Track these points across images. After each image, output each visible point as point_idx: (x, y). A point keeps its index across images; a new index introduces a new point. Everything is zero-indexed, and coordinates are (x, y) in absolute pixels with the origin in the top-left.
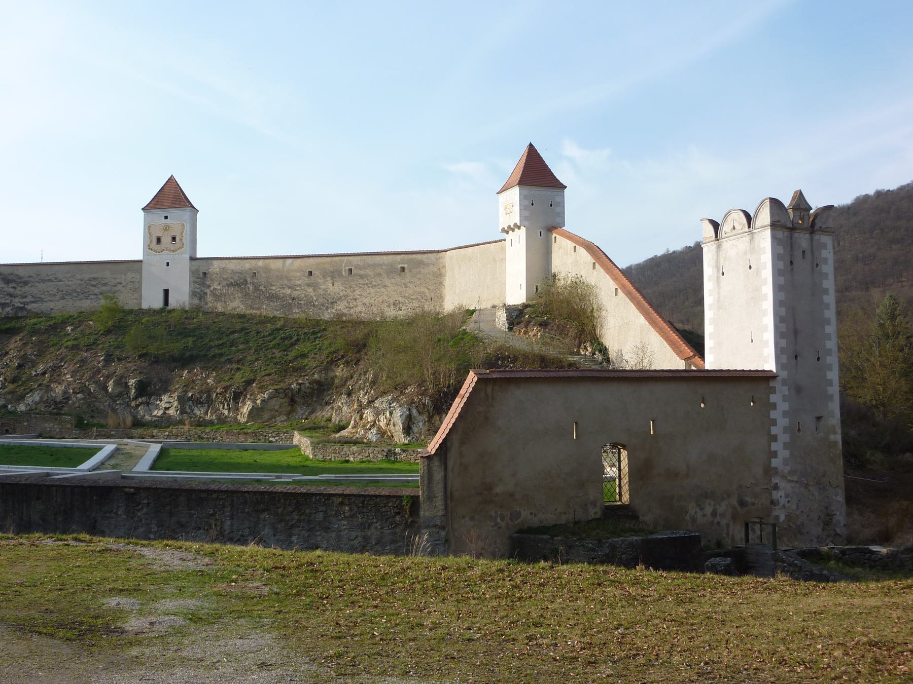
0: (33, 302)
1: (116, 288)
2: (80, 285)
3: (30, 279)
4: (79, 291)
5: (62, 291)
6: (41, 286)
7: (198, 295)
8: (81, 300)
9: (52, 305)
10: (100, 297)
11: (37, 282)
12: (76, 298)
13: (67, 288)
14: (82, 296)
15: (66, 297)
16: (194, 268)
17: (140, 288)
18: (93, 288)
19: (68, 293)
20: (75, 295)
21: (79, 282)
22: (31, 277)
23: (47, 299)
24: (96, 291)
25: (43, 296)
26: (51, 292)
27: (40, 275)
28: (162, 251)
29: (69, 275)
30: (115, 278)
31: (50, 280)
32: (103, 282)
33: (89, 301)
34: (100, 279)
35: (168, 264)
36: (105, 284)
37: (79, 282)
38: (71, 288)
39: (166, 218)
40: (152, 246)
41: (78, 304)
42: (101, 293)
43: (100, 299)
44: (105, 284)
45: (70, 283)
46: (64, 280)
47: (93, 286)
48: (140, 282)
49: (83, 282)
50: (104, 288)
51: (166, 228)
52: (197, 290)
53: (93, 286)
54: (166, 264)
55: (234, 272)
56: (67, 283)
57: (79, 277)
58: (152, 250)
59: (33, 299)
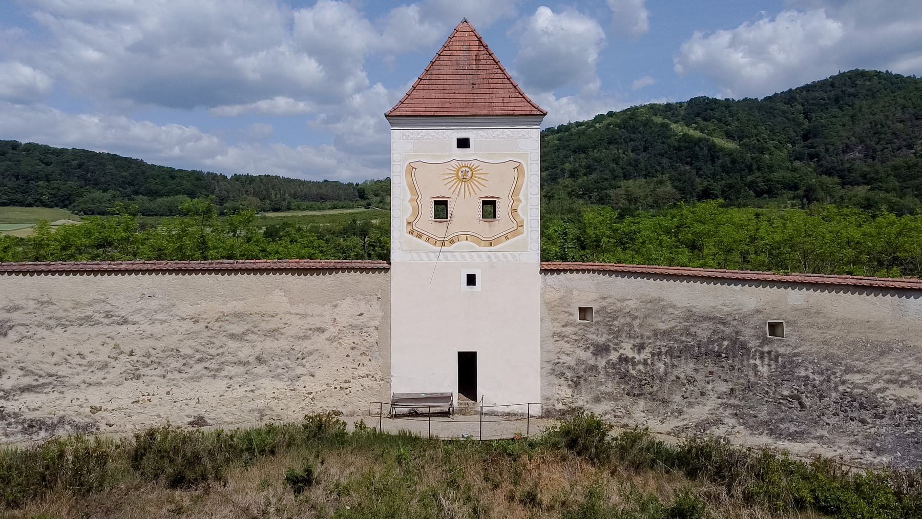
0: (28, 389)
1: (307, 345)
2: (189, 334)
3: (16, 316)
4: (190, 352)
5: (131, 354)
6: (58, 339)
7: (569, 374)
8: (196, 378)
9: (95, 397)
10: (261, 369)
11: (40, 325)
12: (177, 375)
13: (150, 343)
14: (199, 367)
15: (143, 371)
16: (554, 295)
17: (383, 345)
18: (233, 345)
19: (150, 360)
20: (175, 364)
21: (187, 325)
22: (16, 308)
23: (76, 380)
24: (245, 351)
25: (63, 370)
26: (91, 357)
27: (50, 303)
28: (452, 242)
29: (154, 304)
30: (304, 316)
31: (87, 320)
32: (265, 326)
33: (222, 384)
34: (256, 318)
35: (471, 280)
36: (273, 333)
37: (187, 325)
38: (159, 345)
39: (463, 143)
40: (419, 226)
41: (184, 391)
42: (260, 360)
43: (257, 376)
44: (273, 333)
45: (157, 329)
46: (136, 318)
47: (233, 336)
48: (384, 328)
49: (202, 325)
50: (270, 345)
51: (465, 175)
52: (564, 358)
53: (233, 336)
54: (464, 280)
55: (690, 315)
56: (149, 329)
57: (186, 309)
58: (419, 236)
59: (27, 381)
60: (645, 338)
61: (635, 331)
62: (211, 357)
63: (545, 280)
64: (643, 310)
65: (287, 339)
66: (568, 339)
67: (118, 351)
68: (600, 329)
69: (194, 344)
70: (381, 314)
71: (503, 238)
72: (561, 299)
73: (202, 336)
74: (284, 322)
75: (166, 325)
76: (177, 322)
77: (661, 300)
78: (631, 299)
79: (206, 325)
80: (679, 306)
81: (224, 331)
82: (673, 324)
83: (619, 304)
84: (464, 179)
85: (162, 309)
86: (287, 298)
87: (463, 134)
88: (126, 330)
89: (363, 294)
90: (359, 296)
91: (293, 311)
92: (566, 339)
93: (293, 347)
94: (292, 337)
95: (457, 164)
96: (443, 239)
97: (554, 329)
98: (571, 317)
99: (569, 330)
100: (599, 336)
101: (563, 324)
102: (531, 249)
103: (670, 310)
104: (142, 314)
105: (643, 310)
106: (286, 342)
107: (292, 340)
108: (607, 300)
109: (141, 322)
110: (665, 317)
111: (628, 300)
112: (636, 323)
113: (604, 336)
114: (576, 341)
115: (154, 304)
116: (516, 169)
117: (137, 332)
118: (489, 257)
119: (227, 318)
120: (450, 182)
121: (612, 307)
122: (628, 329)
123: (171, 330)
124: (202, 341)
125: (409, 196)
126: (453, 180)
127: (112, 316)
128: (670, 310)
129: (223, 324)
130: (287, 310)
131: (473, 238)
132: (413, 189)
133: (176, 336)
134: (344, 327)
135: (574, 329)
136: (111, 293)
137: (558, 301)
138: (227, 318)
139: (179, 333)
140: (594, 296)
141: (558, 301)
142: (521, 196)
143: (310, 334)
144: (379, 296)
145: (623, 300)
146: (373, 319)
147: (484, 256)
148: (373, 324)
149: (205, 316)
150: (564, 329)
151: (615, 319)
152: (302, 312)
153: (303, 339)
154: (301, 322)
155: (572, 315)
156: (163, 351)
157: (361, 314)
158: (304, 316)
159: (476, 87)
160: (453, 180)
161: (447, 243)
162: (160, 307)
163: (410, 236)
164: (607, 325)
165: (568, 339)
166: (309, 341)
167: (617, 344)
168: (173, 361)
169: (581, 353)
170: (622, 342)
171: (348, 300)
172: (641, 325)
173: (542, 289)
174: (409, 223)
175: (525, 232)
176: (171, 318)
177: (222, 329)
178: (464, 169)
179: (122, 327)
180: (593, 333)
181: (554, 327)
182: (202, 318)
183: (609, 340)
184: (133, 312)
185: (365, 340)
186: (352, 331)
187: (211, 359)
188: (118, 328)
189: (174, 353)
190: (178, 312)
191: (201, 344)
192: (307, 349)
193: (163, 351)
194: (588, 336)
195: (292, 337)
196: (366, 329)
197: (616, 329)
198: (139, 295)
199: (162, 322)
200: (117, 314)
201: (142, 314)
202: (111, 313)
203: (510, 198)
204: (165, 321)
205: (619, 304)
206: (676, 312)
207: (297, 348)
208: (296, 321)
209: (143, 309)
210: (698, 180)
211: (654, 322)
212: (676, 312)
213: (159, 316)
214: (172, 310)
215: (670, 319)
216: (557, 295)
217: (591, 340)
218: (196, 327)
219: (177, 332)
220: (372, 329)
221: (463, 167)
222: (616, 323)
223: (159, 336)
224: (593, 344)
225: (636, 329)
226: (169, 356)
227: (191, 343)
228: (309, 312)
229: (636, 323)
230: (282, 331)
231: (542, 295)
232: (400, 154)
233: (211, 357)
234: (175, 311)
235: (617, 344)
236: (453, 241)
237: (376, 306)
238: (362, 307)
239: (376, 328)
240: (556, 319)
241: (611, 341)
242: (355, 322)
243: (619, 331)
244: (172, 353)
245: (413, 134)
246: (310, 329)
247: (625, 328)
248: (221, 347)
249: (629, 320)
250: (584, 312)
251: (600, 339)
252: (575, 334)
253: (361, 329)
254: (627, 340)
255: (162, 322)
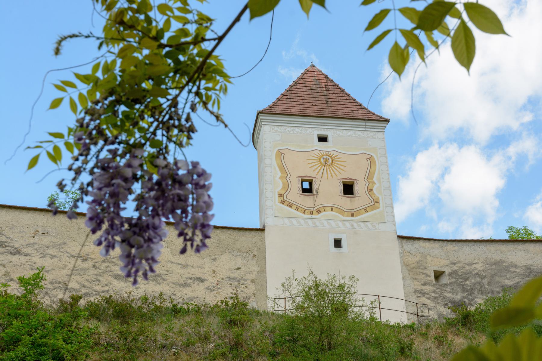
16: (412, 260)
28: (319, 212)
30: (185, 266)
35: (338, 243)
39: (323, 139)
58: (290, 205)
60: (495, 293)
61: (485, 288)
62: (96, 293)
63: (403, 246)
64: (489, 271)
65: (168, 284)
66: (428, 296)
67: (8, 278)
68: (455, 289)
69: (81, 280)
70: (256, 269)
71: (363, 210)
72: (417, 262)
73: (89, 274)
74: (167, 269)
75: (56, 259)
76: (67, 258)
77: (503, 262)
78: (477, 263)
79: (93, 264)
80: (519, 265)
81: (110, 271)
82: (517, 280)
83: (467, 268)
84: (326, 164)
85: (53, 245)
86: (170, 250)
87: (323, 133)
88: (18, 260)
89: (239, 251)
90: (236, 253)
91: (174, 260)
92: (426, 296)
93: (175, 293)
94: (174, 283)
95: (319, 153)
96: (312, 209)
97: (416, 287)
98: (428, 278)
99: (428, 288)
100: (455, 294)
101: (423, 283)
102: (388, 221)
103: (513, 269)
104: (34, 248)
105: (489, 271)
106: (168, 288)
107: (174, 286)
108: (457, 265)
109: (33, 255)
110: (508, 276)
111: (475, 264)
112: (486, 281)
113: (459, 294)
114: (435, 298)
115: (46, 240)
116: (368, 160)
117: (28, 263)
118: (352, 225)
119: (114, 260)
120: (314, 166)
121: (462, 271)
122: (479, 287)
123: (60, 265)
124: (89, 278)
125: (279, 174)
126: (317, 164)
127: (6, 246)
128: (513, 269)
129: (110, 265)
130: (169, 259)
131: (337, 209)
132: (283, 169)
133: (65, 271)
134: (222, 279)
135: (432, 288)
136: (7, 227)
137: (415, 264)
138: (114, 260)
139: (68, 268)
140: (445, 262)
141: (415, 264)
142: (375, 179)
143: (190, 283)
144: (256, 254)
145: (470, 264)
146: (251, 272)
147: (348, 225)
148: (249, 277)
149: (93, 257)
150: (424, 287)
151: (466, 279)
152: (183, 263)
153: (183, 286)
154: (182, 271)
155: (429, 276)
156: (51, 283)
157: (238, 269)
158: (185, 266)
159: (328, 103)
160: (317, 164)
161: (314, 212)
162: (52, 244)
163: (281, 205)
164: (461, 285)
165: (428, 296)
166: (190, 289)
167: (472, 300)
168: (60, 292)
169: (441, 308)
170: (476, 297)
171: (226, 256)
172: (489, 283)
173: (400, 253)
174: (280, 195)
175: (381, 209)
176: (61, 254)
177: (108, 269)
178: (325, 157)
179: (14, 257)
180: (450, 292)
181: (415, 285)
182: (90, 258)
183: (464, 297)
184: (26, 245)
185: (242, 291)
186: (230, 282)
187: (96, 294)
188: (10, 257)
189: (62, 286)
190: (69, 250)
191: (87, 280)
192: (188, 296)
193: (51, 283)
194: (445, 294)
195: (174, 283)
196: (243, 282)
197: (469, 288)
198: (33, 231)
199: (53, 257)
200: (11, 245)
201: (34, 248)
202: (6, 244)
203: (366, 181)
204: (55, 256)
205: (467, 268)
206: (518, 271)
207: (178, 294)
208: (178, 270)
209: (36, 243)
210: (431, 313)
211: (500, 280)
212: (518, 271)
213: (49, 251)
214: (62, 248)
215: (514, 276)
216: (414, 260)
217: (448, 297)
218: (85, 265)
219: (65, 267)
220: (248, 282)
221: (324, 155)
222: (467, 282)
223: (49, 269)
224: (450, 301)
225: (486, 286)
226: (57, 288)
227: (77, 278)
228: (189, 263)
229: (486, 281)
230: (165, 277)
231: (402, 257)
232: (270, 143)
233: (96, 293)
234: (65, 248)
235: (472, 300)
236: (319, 210)
237: (253, 262)
238: (239, 262)
239: (253, 281)
240: (416, 279)
241: (466, 298)
242: (232, 275)
243: (472, 289)
244: (60, 285)
245: (280, 129)
246: (191, 278)
247: (477, 286)
248: (107, 285)
249: (478, 279)
250: (438, 275)
251: (456, 297)
252: (433, 292)
253: (239, 281)
254: (480, 296)
255: (53, 257)
